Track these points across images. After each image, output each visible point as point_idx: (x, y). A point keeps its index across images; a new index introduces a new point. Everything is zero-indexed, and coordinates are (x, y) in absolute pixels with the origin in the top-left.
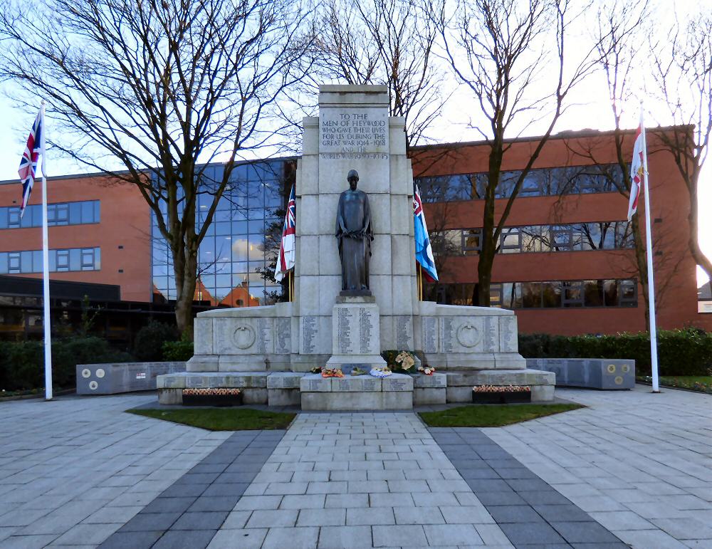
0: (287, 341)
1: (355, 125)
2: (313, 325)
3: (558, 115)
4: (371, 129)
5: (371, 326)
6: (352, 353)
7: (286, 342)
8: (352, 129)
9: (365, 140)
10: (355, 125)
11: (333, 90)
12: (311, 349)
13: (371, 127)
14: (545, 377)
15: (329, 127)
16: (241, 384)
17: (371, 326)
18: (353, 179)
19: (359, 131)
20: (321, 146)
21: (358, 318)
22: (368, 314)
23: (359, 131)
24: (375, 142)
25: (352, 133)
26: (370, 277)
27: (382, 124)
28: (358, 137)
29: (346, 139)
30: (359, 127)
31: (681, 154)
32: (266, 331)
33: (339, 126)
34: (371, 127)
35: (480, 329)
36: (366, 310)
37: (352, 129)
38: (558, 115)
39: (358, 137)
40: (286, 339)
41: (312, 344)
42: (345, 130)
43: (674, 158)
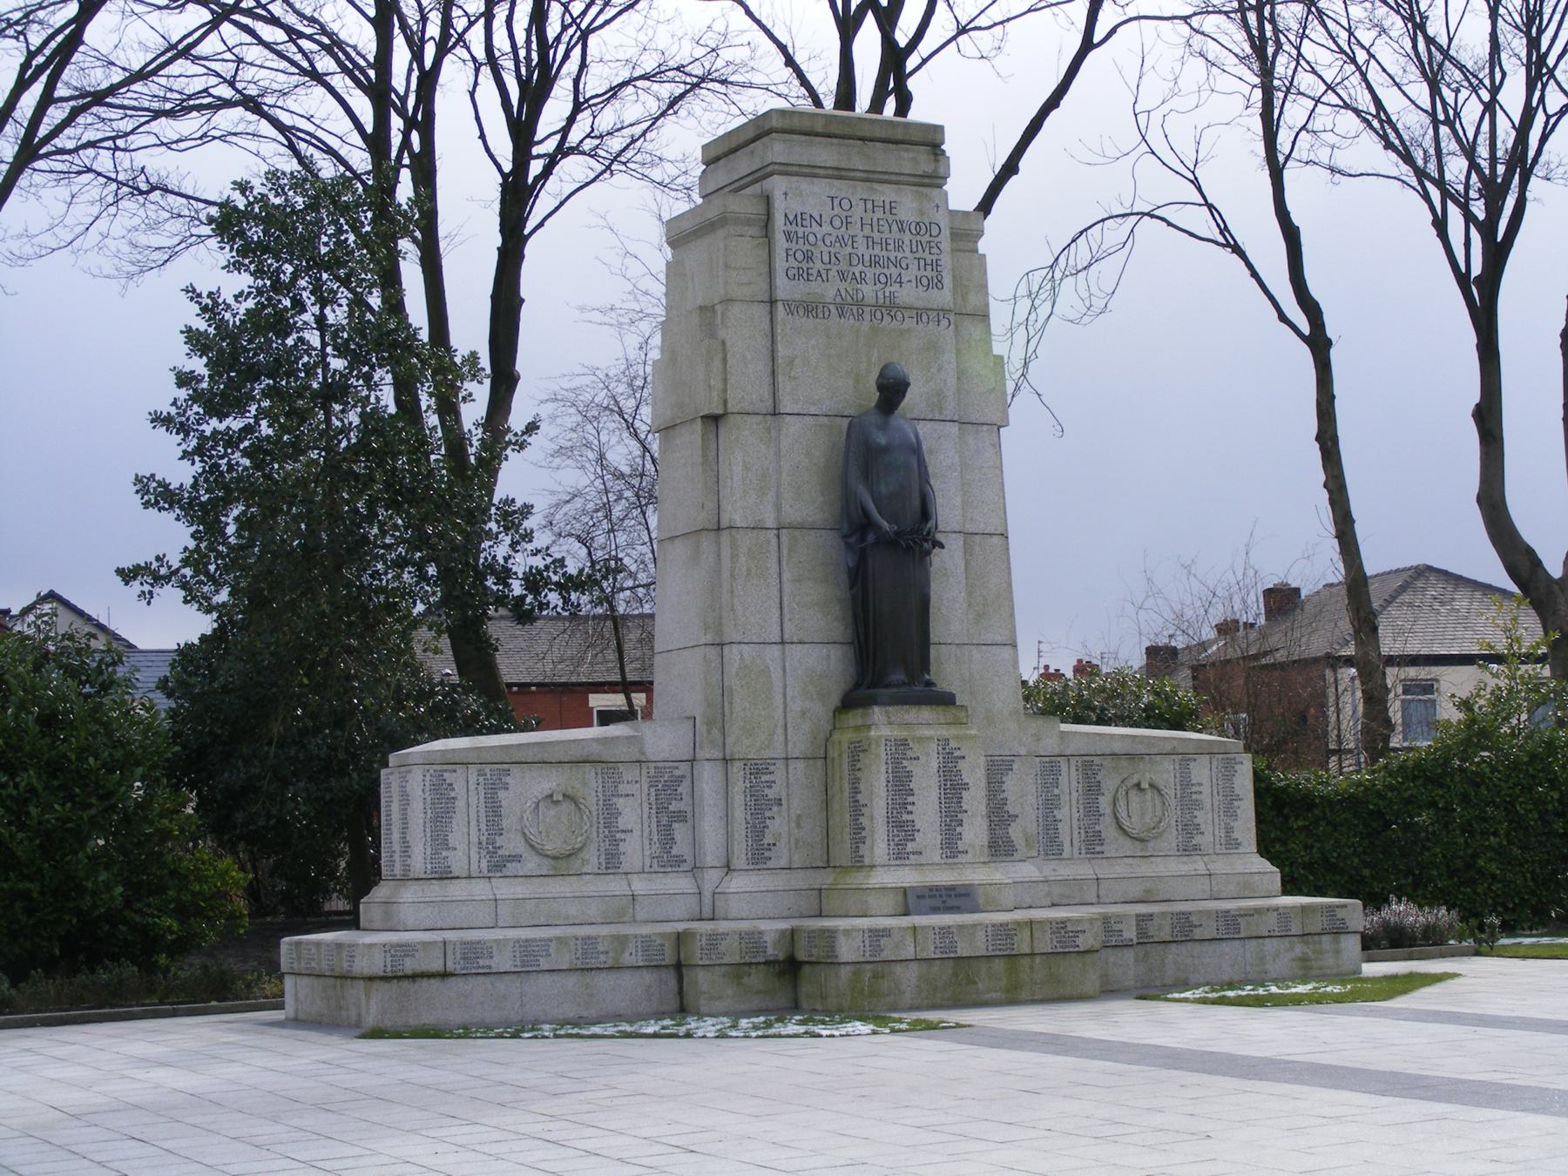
0: (680, 831)
1: (867, 230)
2: (770, 784)
3: (1087, 45)
4: (907, 242)
5: (966, 787)
6: (922, 859)
7: (678, 836)
8: (860, 240)
9: (894, 271)
10: (867, 230)
11: (847, 131)
12: (767, 854)
13: (907, 237)
14: (1340, 914)
15: (800, 231)
16: (603, 958)
17: (966, 787)
18: (892, 391)
19: (877, 248)
20: (781, 281)
21: (935, 765)
22: (957, 753)
23: (877, 248)
24: (919, 281)
25: (861, 248)
26: (933, 650)
27: (935, 231)
28: (874, 262)
29: (844, 266)
30: (876, 235)
31: (1451, 206)
32: (620, 803)
33: (826, 228)
34: (907, 237)
35: (1169, 792)
36: (953, 744)
37: (860, 240)
38: (1087, 45)
39: (874, 262)
40: (675, 825)
41: (768, 839)
42: (840, 240)
43: (1431, 218)
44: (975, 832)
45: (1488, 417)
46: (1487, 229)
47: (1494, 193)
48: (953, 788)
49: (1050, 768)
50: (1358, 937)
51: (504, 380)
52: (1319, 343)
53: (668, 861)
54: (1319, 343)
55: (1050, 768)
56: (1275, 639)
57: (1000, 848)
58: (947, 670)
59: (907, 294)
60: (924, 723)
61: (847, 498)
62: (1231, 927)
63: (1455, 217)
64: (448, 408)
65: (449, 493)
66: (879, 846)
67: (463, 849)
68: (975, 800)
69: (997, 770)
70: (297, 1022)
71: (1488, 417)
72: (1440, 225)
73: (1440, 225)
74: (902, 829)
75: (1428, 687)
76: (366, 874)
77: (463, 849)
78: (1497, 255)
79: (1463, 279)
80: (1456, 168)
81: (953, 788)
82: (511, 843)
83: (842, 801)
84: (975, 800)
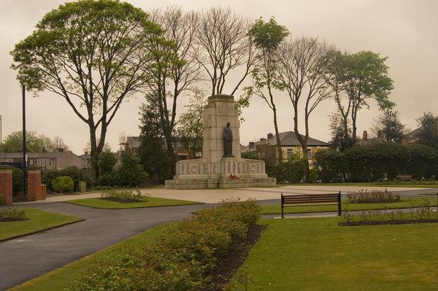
3: (247, 74)
18: (229, 125)
38: (247, 74)
44: (236, 170)
45: (296, 119)
46: (296, 96)
47: (297, 90)
48: (234, 166)
49: (244, 164)
50: (29, 94)
51: (174, 114)
52: (274, 110)
53: (205, 173)
54: (274, 110)
55: (244, 164)
56: (270, 142)
57: (239, 172)
58: (233, 154)
59: (230, 114)
60: (231, 159)
61: (224, 136)
62: (262, 180)
63: (292, 93)
64: (167, 118)
65: (168, 127)
66: (227, 171)
67: (185, 171)
68: (236, 167)
69: (239, 164)
70: (167, 189)
71: (296, 119)
72: (290, 95)
73: (290, 95)
74: (229, 170)
75: (291, 150)
76: (174, 173)
77: (185, 171)
78: (297, 99)
79: (293, 102)
80: (292, 87)
81: (234, 166)
82: (190, 171)
83: (223, 167)
84: (236, 167)
